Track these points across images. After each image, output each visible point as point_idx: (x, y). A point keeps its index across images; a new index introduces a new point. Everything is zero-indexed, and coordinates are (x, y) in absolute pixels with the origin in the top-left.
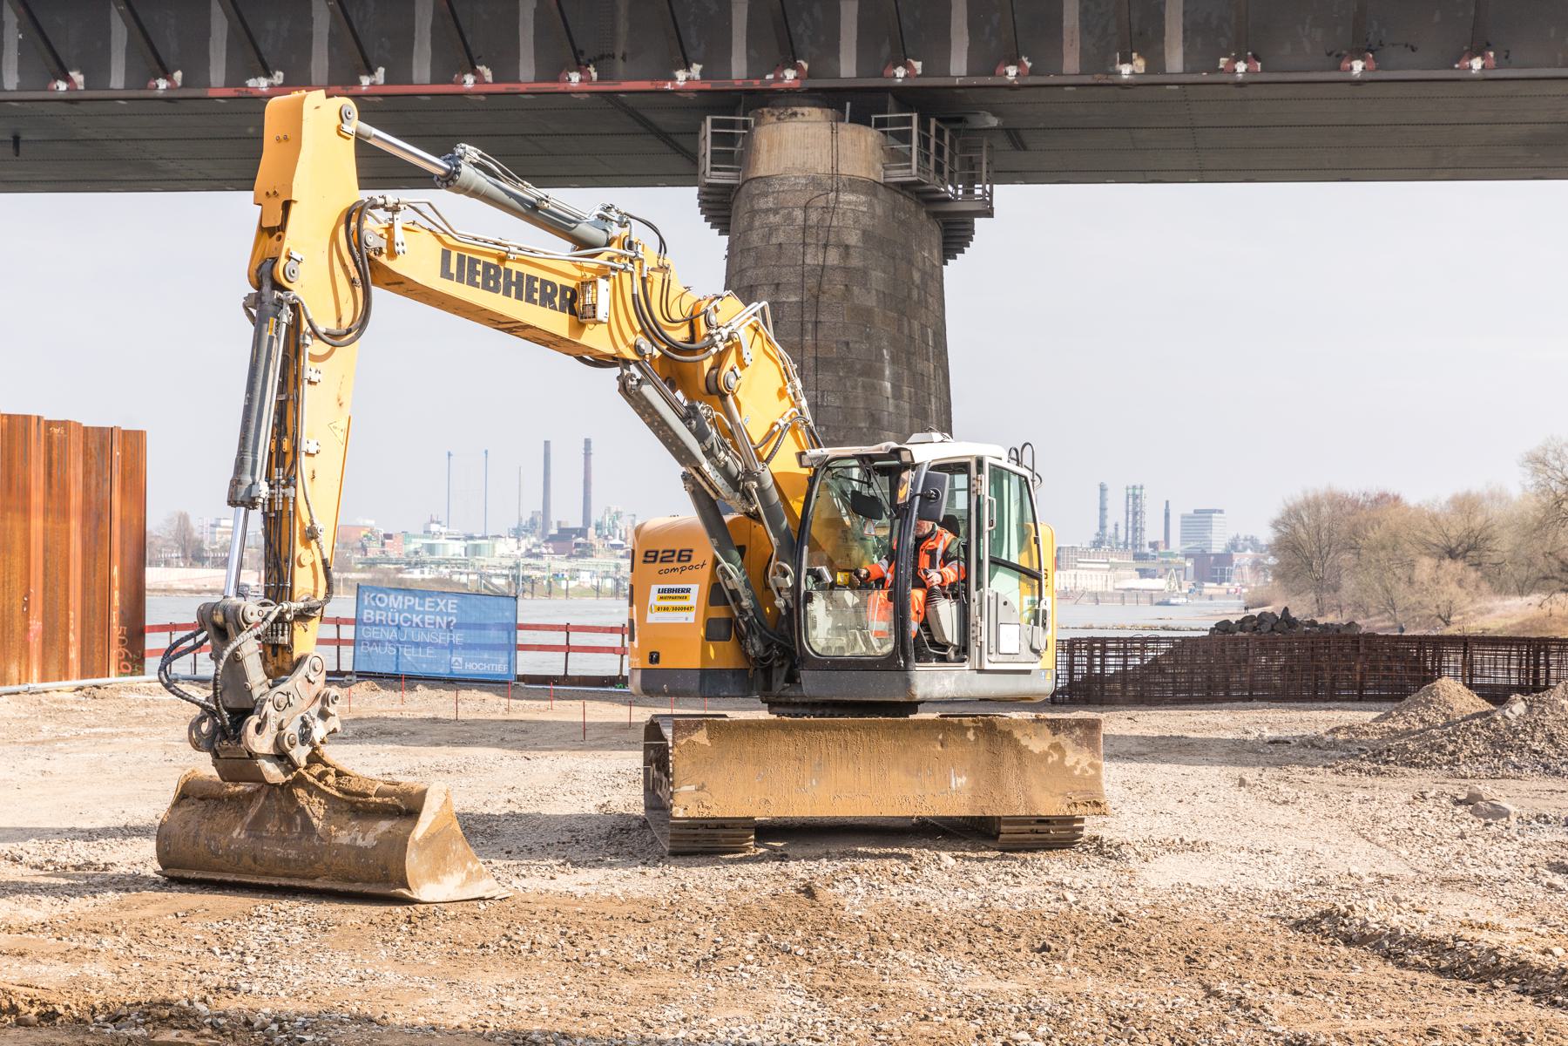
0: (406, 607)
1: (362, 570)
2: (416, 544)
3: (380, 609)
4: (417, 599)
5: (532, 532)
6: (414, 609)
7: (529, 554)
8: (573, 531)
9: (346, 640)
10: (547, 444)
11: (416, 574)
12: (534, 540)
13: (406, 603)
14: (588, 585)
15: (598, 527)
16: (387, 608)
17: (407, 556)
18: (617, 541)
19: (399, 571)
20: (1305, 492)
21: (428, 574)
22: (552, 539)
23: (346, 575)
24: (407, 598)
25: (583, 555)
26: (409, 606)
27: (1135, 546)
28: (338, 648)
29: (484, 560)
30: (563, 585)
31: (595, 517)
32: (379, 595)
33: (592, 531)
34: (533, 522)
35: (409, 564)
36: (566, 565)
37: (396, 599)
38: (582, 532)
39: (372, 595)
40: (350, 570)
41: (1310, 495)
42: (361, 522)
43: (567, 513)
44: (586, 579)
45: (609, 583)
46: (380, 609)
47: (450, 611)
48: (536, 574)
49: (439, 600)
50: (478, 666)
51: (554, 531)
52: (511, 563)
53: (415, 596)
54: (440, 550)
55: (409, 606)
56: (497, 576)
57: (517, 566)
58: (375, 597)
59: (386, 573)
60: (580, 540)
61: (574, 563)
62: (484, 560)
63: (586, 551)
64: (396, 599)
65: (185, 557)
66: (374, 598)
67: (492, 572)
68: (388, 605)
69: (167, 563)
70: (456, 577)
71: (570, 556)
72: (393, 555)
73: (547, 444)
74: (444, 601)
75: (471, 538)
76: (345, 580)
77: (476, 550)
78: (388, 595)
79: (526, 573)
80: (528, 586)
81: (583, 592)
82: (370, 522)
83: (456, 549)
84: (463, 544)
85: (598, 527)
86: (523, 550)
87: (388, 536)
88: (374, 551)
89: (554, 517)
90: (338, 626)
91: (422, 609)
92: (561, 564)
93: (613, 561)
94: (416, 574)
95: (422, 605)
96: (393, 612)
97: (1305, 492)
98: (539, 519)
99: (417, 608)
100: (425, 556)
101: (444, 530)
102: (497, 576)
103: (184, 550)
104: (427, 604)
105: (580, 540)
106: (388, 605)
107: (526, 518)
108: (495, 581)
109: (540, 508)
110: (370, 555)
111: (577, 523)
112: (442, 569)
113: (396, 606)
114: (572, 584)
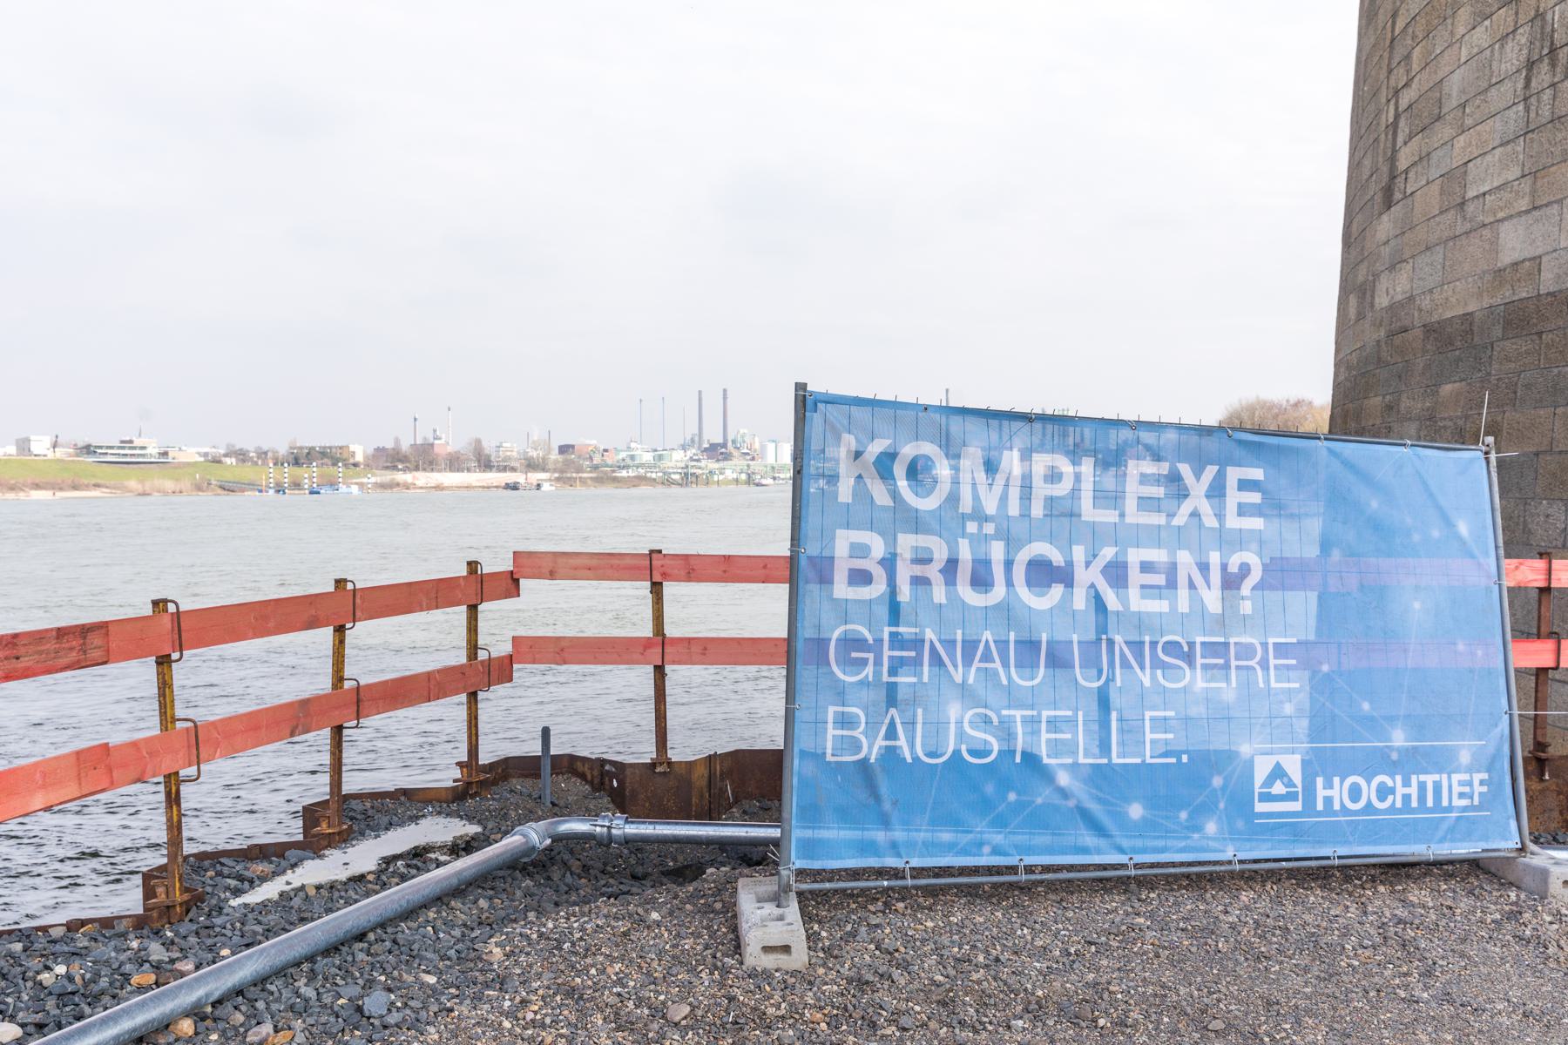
0: (1037, 510)
1: (590, 472)
2: (623, 455)
3: (916, 523)
4: (1087, 467)
5: (693, 447)
6: (1073, 514)
7: (692, 459)
8: (719, 445)
9: (689, 641)
10: (700, 392)
11: (624, 473)
12: (694, 451)
13: (1041, 490)
14: (730, 478)
15: (734, 442)
16: (951, 518)
17: (618, 462)
18: (745, 451)
19: (614, 471)
20: (1258, 397)
21: (631, 473)
22: (706, 450)
23: (580, 475)
24: (1041, 463)
25: (725, 459)
26: (1050, 501)
27: (1064, 446)
28: (660, 671)
29: (666, 463)
30: (716, 478)
31: (730, 438)
32: (908, 451)
33: (730, 444)
34: (693, 441)
35: (619, 467)
36: (716, 466)
37: (991, 467)
38: (724, 445)
39: (875, 448)
40: (583, 472)
41: (1244, 402)
42: (588, 442)
43: (713, 435)
44: (730, 475)
45: (744, 477)
46: (916, 523)
47: (1233, 522)
48: (699, 472)
49: (1185, 469)
50: (1369, 792)
51: (706, 445)
52: (683, 465)
53: (1075, 454)
54: (638, 458)
55: (1050, 501)
56: (674, 473)
57: (687, 467)
58: (889, 457)
59: (606, 473)
60: (723, 450)
61: (721, 464)
62: (666, 463)
63: (727, 457)
64: (991, 467)
65: (480, 466)
66: (884, 464)
67: (671, 471)
68: (953, 499)
69: (469, 470)
70: (648, 475)
71: (718, 460)
72: (609, 462)
73: (700, 392)
74: (1210, 471)
75: (656, 451)
76: (580, 478)
77: (660, 457)
78: (952, 451)
79: (693, 471)
80: (694, 479)
81: (728, 482)
82: (594, 442)
83: (648, 457)
84: (652, 454)
85: (734, 442)
86: (688, 457)
87: (606, 450)
88: (597, 460)
89: (706, 437)
90: (656, 589)
91: (1109, 516)
92: (713, 465)
93: (746, 463)
94: (624, 473)
95: (1110, 498)
96: (980, 540)
97: (1258, 397)
98: (697, 439)
99: (1088, 510)
100: (629, 462)
101: (639, 446)
102: (674, 473)
103: (479, 461)
104: (1133, 489)
105: (723, 450)
106: (953, 499)
107: (689, 438)
108: (673, 476)
109: (697, 432)
110: (595, 462)
111: (720, 440)
112: (640, 470)
113: (991, 507)
114: (721, 477)
